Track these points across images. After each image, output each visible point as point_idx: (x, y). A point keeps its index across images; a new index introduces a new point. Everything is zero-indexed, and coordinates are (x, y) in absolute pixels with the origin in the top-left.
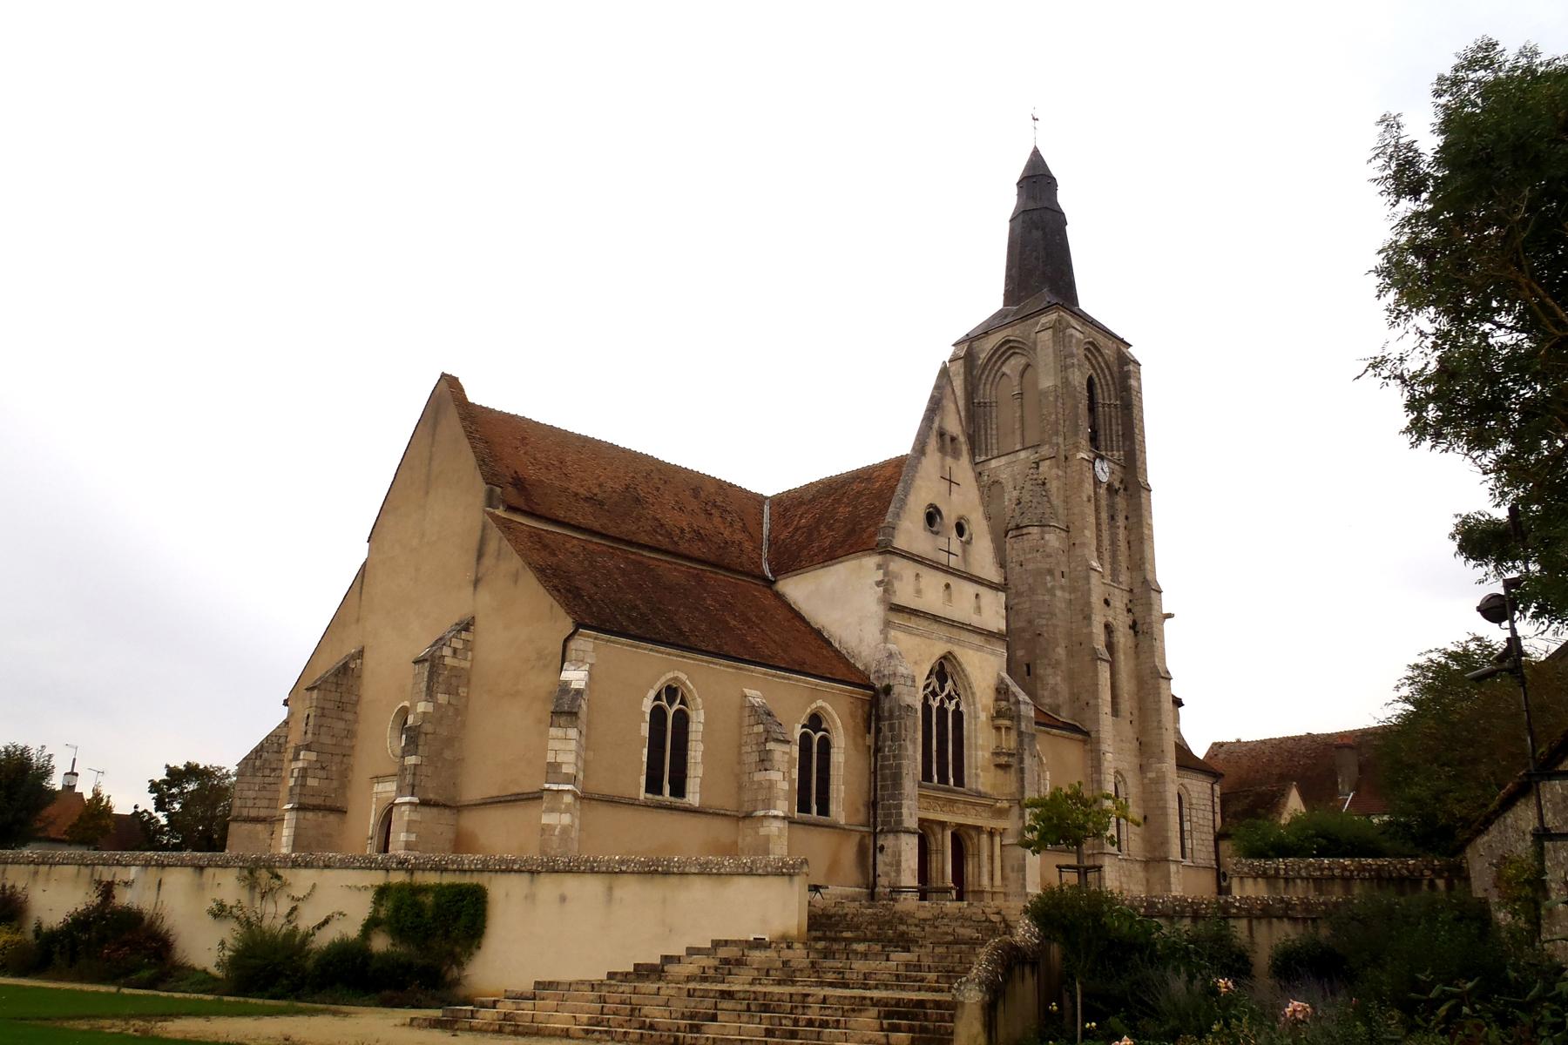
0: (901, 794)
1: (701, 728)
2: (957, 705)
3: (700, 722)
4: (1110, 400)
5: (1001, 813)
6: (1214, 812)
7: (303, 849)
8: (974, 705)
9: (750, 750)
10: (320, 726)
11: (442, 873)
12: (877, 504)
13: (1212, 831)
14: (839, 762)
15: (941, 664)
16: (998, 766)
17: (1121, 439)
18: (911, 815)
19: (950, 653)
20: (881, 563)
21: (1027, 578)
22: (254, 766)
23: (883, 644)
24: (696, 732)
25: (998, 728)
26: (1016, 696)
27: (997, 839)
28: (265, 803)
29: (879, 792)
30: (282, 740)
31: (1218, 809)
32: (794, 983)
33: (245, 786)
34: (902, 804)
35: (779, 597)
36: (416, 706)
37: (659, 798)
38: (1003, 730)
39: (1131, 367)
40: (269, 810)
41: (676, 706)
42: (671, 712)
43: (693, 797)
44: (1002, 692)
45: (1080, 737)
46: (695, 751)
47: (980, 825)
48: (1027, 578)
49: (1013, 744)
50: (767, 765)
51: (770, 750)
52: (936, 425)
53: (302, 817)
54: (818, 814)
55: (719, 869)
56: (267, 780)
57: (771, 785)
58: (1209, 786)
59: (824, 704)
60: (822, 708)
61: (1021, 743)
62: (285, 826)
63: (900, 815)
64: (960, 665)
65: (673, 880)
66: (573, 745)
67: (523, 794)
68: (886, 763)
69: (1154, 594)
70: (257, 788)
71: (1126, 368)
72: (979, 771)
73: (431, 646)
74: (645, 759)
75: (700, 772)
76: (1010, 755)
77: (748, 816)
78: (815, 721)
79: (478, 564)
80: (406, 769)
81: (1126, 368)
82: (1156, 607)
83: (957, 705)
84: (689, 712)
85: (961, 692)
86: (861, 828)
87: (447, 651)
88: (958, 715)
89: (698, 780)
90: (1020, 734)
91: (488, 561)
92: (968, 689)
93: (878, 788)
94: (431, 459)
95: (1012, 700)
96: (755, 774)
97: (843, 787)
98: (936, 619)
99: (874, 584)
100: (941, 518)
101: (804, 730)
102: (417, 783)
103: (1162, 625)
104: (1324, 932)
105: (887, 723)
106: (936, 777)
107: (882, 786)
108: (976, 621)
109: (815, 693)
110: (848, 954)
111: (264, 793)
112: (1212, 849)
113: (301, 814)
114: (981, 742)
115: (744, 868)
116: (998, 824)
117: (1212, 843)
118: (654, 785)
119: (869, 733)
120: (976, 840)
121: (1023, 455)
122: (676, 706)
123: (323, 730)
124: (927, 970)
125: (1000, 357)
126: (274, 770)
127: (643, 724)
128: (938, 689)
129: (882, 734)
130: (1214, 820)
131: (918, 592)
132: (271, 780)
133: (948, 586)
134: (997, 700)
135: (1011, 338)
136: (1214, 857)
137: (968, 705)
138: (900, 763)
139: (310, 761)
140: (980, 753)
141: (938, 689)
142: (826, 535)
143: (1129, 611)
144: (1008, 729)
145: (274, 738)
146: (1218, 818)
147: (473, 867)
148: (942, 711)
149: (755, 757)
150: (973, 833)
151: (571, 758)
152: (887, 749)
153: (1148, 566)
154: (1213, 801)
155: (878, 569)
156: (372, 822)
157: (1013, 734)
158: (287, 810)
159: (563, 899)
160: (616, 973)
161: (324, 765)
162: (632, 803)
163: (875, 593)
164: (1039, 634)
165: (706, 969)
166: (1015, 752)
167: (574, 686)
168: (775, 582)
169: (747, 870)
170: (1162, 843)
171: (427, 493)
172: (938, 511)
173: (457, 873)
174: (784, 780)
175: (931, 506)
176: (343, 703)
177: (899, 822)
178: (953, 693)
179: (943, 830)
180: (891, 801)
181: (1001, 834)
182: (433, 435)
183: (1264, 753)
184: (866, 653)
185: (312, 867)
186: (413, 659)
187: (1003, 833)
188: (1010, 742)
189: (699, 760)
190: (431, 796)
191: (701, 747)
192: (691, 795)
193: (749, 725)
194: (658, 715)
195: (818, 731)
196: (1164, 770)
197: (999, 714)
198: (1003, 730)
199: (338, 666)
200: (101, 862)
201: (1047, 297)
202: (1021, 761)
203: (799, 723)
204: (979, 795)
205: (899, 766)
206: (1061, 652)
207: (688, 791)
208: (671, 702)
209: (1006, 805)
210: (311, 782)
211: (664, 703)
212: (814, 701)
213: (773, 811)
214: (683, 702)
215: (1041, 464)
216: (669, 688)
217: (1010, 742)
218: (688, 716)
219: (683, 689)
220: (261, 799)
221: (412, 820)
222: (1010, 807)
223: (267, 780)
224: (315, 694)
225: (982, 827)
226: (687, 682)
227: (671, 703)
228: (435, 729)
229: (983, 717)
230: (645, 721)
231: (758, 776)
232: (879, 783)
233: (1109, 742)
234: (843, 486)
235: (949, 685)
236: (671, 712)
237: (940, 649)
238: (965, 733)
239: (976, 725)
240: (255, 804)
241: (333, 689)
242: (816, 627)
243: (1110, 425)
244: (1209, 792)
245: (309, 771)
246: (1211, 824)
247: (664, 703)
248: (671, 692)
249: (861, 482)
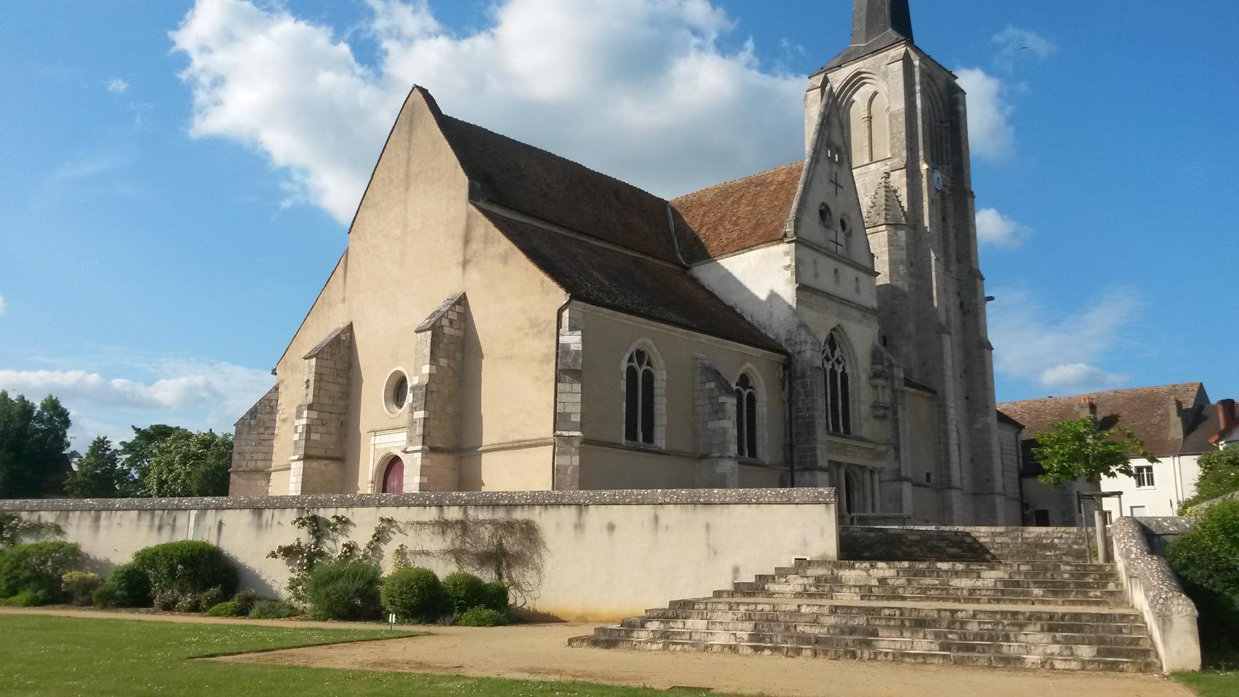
1: (664, 384)
3: (663, 380)
5: (879, 456)
6: (1018, 456)
7: (310, 493)
8: (857, 368)
10: (319, 390)
12: (776, 203)
13: (1016, 470)
14: (763, 414)
15: (831, 334)
16: (876, 417)
17: (950, 155)
18: (823, 456)
19: (839, 325)
20: (788, 250)
21: (883, 267)
23: (792, 318)
24: (661, 388)
25: (875, 387)
27: (876, 477)
28: (261, 456)
29: (794, 438)
30: (273, 403)
33: (243, 443)
35: (695, 281)
36: (421, 368)
39: (959, 95)
40: (265, 462)
41: (645, 367)
43: (660, 441)
44: (876, 357)
46: (661, 404)
47: (864, 464)
48: (883, 267)
50: (720, 415)
51: (723, 403)
56: (263, 437)
57: (724, 431)
58: (1014, 435)
60: (749, 369)
61: (895, 399)
63: (815, 456)
64: (846, 334)
65: (718, 509)
66: (578, 398)
67: (525, 441)
69: (978, 281)
70: (253, 444)
71: (954, 96)
72: (862, 422)
73: (430, 318)
75: (665, 422)
76: (886, 408)
77: (705, 457)
78: (744, 380)
80: (416, 422)
81: (954, 96)
82: (979, 291)
85: (847, 358)
86: (781, 468)
87: (445, 322)
88: (844, 376)
89: (664, 428)
90: (894, 391)
91: (475, 246)
92: (852, 355)
94: (409, 161)
95: (886, 364)
96: (709, 423)
98: (830, 296)
100: (830, 215)
101: (737, 387)
103: (985, 306)
104: (857, 565)
105: (799, 381)
109: (745, 358)
112: (1017, 485)
113: (308, 463)
114: (863, 395)
116: (878, 464)
117: (1017, 481)
118: (631, 435)
119: (784, 390)
121: (873, 166)
122: (645, 367)
123: (322, 392)
125: (851, 88)
126: (267, 428)
128: (830, 355)
130: (1018, 462)
131: (816, 275)
132: (265, 437)
133: (836, 271)
134: (873, 364)
135: (863, 70)
136: (1018, 492)
138: (814, 414)
140: (863, 407)
141: (830, 355)
143: (958, 294)
144: (883, 387)
145: (266, 402)
147: (523, 502)
148: (833, 372)
149: (708, 409)
150: (858, 471)
151: (578, 409)
153: (973, 259)
154: (1017, 446)
155: (785, 256)
156: (371, 469)
157: (888, 392)
159: (611, 527)
161: (324, 422)
162: (616, 446)
164: (894, 312)
166: (889, 406)
168: (687, 269)
169: (785, 500)
171: (407, 189)
172: (827, 208)
173: (526, 507)
174: (734, 428)
175: (823, 204)
176: (337, 370)
177: (816, 462)
178: (840, 359)
181: (879, 472)
182: (410, 140)
183: (1016, 412)
184: (776, 325)
187: (881, 471)
188: (886, 397)
189: (664, 411)
190: (438, 445)
191: (665, 400)
192: (658, 440)
193: (701, 383)
194: (631, 372)
195: (747, 388)
196: (989, 422)
197: (876, 375)
198: (880, 389)
199: (331, 338)
202: (895, 413)
205: (812, 416)
207: (655, 437)
208: (640, 363)
209: (883, 448)
211: (635, 364)
212: (743, 363)
213: (569, 471)
214: (649, 364)
215: (892, 173)
216: (638, 351)
217: (886, 397)
218: (654, 376)
219: (650, 352)
220: (257, 453)
221: (425, 466)
223: (263, 437)
224: (314, 361)
225: (865, 466)
229: (864, 377)
230: (623, 379)
233: (952, 399)
234: (740, 190)
235: (837, 353)
237: (832, 322)
239: (858, 384)
240: (252, 457)
241: (329, 358)
242: (729, 304)
244: (1014, 440)
245: (312, 427)
246: (1016, 465)
248: (640, 355)
249: (757, 186)
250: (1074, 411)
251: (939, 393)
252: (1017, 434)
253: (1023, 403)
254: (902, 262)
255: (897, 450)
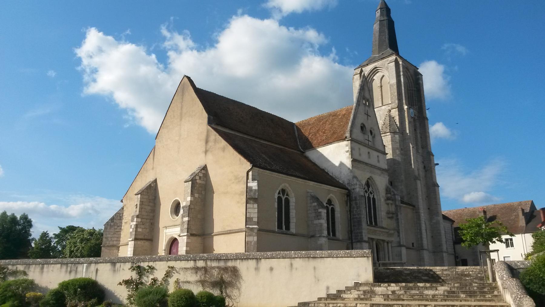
0: (361, 228)
1: (294, 204)
2: (373, 196)
3: (293, 202)
4: (412, 88)
5: (391, 235)
6: (453, 235)
9: (311, 212)
11: (219, 261)
13: (452, 241)
16: (389, 218)
19: (371, 177)
20: (347, 144)
22: (111, 225)
25: (388, 204)
26: (394, 192)
27: (390, 245)
29: (352, 228)
31: (454, 234)
32: (436, 300)
34: (362, 232)
35: (307, 158)
37: (282, 230)
38: (390, 205)
39: (420, 76)
41: (285, 196)
42: (283, 199)
44: (388, 191)
45: (411, 207)
46: (293, 213)
49: (393, 210)
52: (362, 95)
53: (136, 243)
54: (333, 236)
55: (337, 255)
56: (116, 230)
57: (321, 225)
58: (450, 225)
59: (333, 195)
60: (332, 197)
61: (397, 209)
62: (129, 247)
63: (362, 236)
65: (319, 260)
66: (256, 210)
68: (355, 217)
69: (431, 157)
70: (112, 233)
71: (418, 77)
72: (382, 220)
74: (277, 216)
76: (393, 214)
77: (313, 236)
78: (330, 202)
79: (206, 145)
83: (373, 196)
84: (289, 198)
87: (197, 178)
88: (374, 199)
90: (396, 206)
91: (211, 144)
93: (352, 226)
95: (392, 194)
97: (340, 226)
98: (366, 164)
99: (345, 152)
100: (365, 128)
102: (189, 228)
105: (354, 202)
106: (374, 223)
107: (354, 226)
108: (378, 165)
109: (329, 192)
110: (418, 288)
111: (115, 235)
112: (453, 248)
114: (382, 208)
115: (347, 254)
117: (453, 246)
118: (280, 227)
119: (347, 206)
120: (383, 245)
121: (383, 107)
122: (285, 196)
123: (143, 210)
124: (457, 293)
126: (118, 226)
127: (276, 203)
128: (367, 190)
129: (352, 206)
131: (360, 155)
132: (118, 230)
133: (369, 153)
134: (386, 194)
135: (377, 66)
137: (377, 196)
139: (138, 222)
141: (367, 190)
142: (323, 135)
144: (391, 204)
145: (118, 215)
146: (454, 236)
147: (232, 258)
148: (369, 198)
151: (256, 215)
152: (355, 212)
157: (393, 206)
158: (130, 241)
159: (271, 269)
160: (322, 298)
162: (274, 232)
163: (346, 155)
165: (360, 296)
166: (394, 212)
167: (254, 188)
170: (439, 246)
171: (181, 120)
172: (364, 125)
177: (362, 238)
178: (372, 192)
179: (372, 242)
180: (358, 231)
181: (391, 243)
182: (182, 99)
185: (163, 261)
186: (184, 181)
187: (391, 242)
188: (392, 209)
189: (294, 216)
190: (194, 232)
194: (279, 199)
197: (388, 199)
198: (390, 205)
200: (57, 263)
201: (389, 51)
202: (397, 216)
203: (325, 202)
204: (383, 228)
206: (403, 177)
209: (392, 232)
210: (139, 230)
211: (281, 195)
214: (287, 195)
217: (392, 209)
220: (114, 238)
222: (394, 233)
223: (116, 230)
226: (289, 187)
227: (283, 195)
228: (194, 207)
229: (383, 200)
231: (316, 222)
232: (352, 224)
233: (422, 209)
235: (370, 189)
236: (283, 199)
237: (368, 175)
238: (377, 206)
240: (111, 240)
242: (322, 168)
243: (413, 97)
244: (450, 227)
246: (452, 239)
247: (281, 195)
249: (333, 116)
250: (476, 214)
251: (416, 206)
252: (451, 225)
253: (454, 211)
254: (397, 148)
255: (399, 232)
